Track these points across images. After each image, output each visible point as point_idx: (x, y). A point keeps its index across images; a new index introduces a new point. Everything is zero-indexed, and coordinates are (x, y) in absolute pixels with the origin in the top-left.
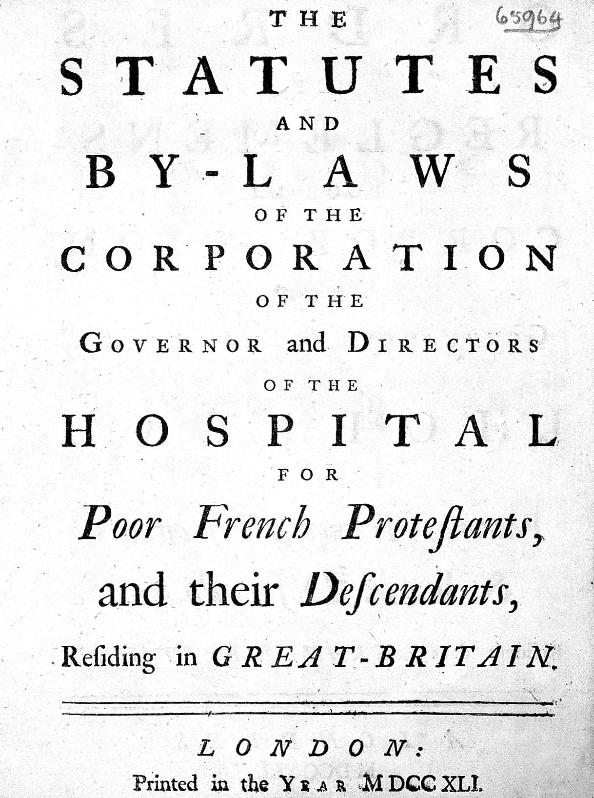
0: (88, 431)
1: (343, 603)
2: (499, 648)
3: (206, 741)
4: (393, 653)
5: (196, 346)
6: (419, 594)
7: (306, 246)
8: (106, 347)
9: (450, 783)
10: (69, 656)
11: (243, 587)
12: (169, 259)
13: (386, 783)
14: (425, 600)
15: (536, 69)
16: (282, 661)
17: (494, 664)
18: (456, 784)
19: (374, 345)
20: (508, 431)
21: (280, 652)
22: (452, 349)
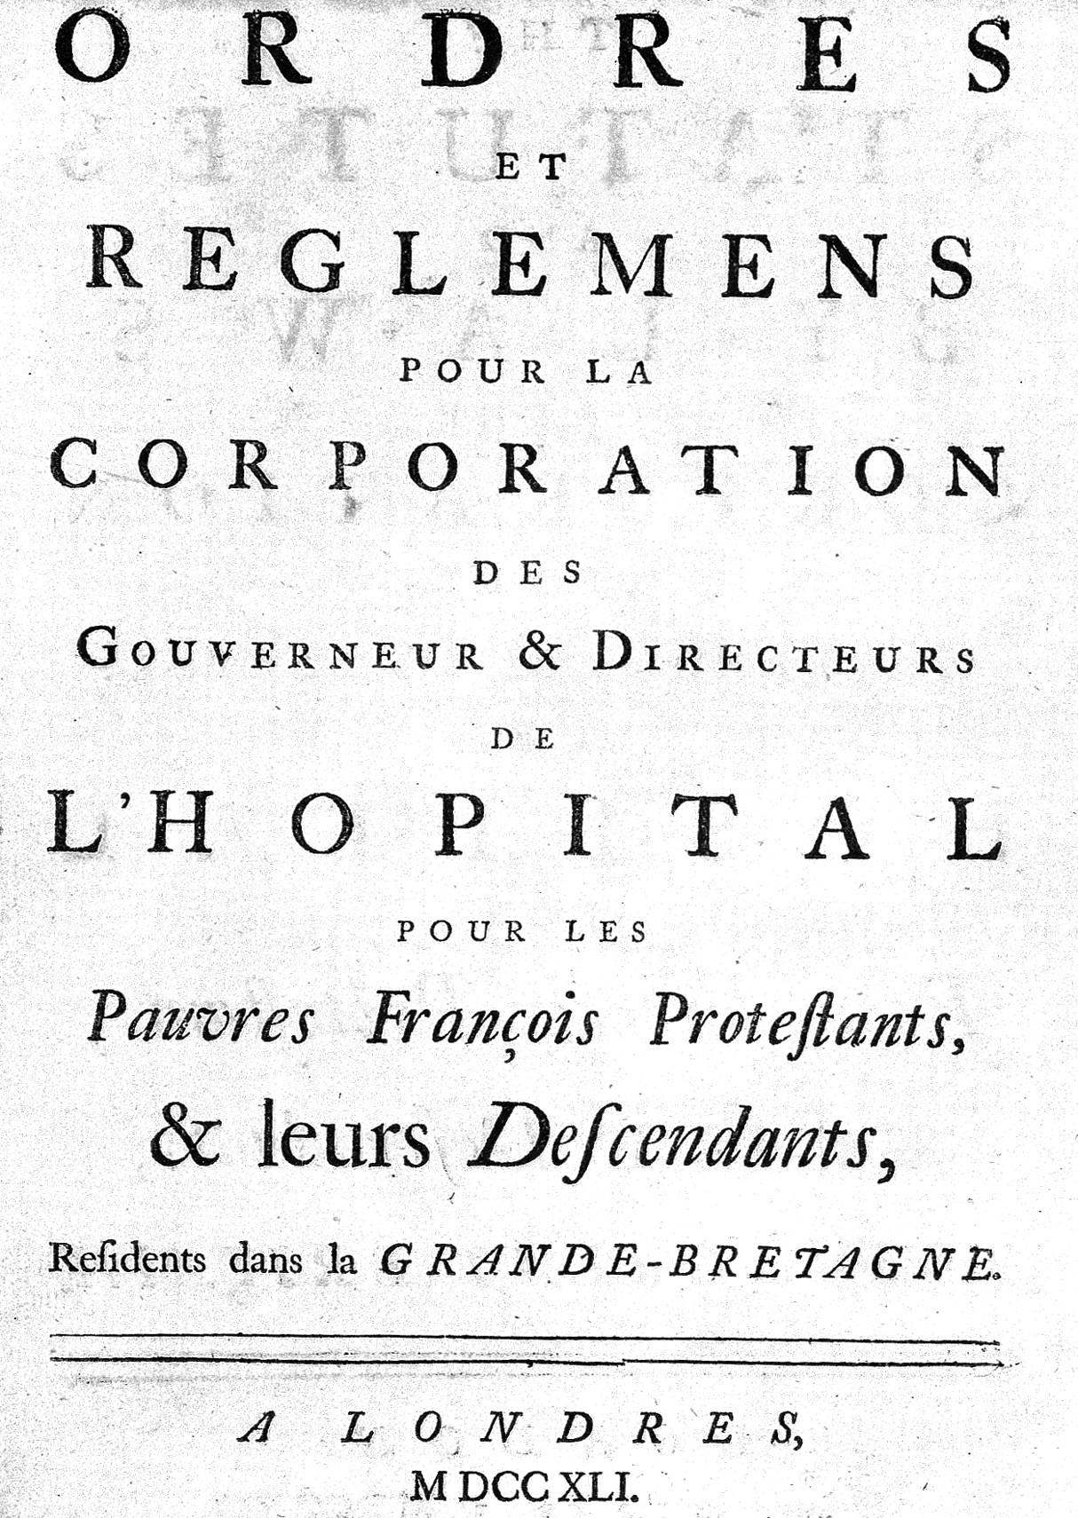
0: (199, 820)
1: (557, 1161)
2: (500, 1248)
3: (356, 1415)
4: (694, 1255)
5: (321, 656)
6: (704, 1146)
7: (355, 444)
8: (123, 654)
9: (573, 1486)
10: (61, 1256)
11: (305, 1131)
12: (262, 465)
13: (453, 1486)
14: (715, 1157)
15: (1006, 63)
16: (766, 1269)
17: (849, 1275)
18: (585, 1487)
19: (639, 656)
20: (904, 830)
21: (763, 1255)
22: (768, 666)
